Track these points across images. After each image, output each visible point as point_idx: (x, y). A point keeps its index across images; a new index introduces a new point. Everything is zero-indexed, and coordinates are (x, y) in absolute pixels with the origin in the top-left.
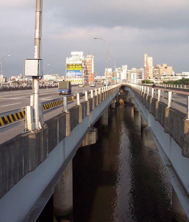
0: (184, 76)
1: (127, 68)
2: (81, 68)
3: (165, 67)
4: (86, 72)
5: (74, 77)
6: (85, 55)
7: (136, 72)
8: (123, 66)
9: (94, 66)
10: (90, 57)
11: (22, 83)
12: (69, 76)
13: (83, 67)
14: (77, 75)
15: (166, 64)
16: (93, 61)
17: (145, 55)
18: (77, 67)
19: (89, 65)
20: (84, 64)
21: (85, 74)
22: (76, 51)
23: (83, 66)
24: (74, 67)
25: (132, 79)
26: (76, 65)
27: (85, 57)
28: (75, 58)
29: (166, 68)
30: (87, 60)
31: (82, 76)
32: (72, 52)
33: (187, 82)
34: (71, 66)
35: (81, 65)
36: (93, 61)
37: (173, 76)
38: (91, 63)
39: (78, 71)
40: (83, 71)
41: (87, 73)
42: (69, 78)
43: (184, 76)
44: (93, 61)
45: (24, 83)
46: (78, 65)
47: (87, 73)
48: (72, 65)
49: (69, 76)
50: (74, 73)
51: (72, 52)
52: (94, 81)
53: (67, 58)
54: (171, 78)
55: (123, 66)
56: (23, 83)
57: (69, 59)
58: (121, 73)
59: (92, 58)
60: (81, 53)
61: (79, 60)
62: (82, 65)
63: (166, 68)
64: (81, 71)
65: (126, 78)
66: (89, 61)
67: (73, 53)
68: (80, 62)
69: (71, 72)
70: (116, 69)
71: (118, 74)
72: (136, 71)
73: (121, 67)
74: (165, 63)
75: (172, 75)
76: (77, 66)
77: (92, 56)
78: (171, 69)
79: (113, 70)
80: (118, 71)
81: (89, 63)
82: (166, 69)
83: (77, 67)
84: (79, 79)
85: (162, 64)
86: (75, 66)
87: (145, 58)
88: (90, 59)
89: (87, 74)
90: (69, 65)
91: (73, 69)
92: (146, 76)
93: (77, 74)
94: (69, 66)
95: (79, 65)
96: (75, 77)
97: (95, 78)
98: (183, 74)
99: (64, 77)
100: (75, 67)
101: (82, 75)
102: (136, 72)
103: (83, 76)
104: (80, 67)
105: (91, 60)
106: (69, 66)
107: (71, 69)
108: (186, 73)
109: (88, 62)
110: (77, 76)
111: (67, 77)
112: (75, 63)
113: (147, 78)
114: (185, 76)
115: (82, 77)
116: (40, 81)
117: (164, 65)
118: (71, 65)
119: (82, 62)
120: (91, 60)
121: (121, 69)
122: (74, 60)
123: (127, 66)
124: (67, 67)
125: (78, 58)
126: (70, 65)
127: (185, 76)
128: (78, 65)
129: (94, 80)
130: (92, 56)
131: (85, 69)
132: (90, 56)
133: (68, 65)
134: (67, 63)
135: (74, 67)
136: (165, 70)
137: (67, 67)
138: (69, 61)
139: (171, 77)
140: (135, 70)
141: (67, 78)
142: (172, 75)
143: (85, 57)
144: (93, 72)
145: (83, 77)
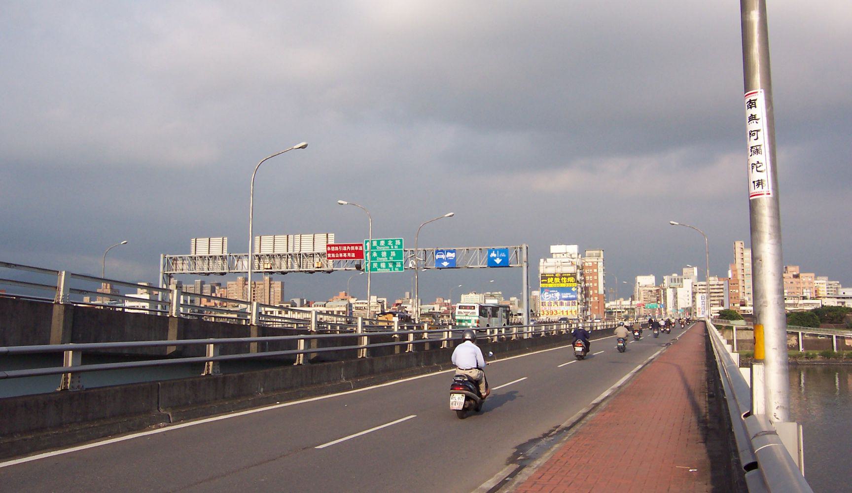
0: (844, 298)
1: (696, 274)
2: (575, 282)
3: (795, 273)
4: (584, 292)
5: (558, 304)
6: (582, 253)
7: (718, 287)
8: (685, 270)
9: (604, 277)
10: (594, 255)
11: (440, 317)
12: (547, 302)
13: (578, 281)
14: (565, 299)
15: (798, 267)
16: (602, 263)
17: (738, 245)
18: (565, 281)
19: (590, 274)
20: (582, 274)
21: (583, 297)
22: (561, 244)
23: (579, 277)
24: (557, 280)
25: (698, 306)
26: (561, 276)
27: (584, 256)
28: (560, 259)
29: (796, 276)
30: (589, 262)
31: (576, 301)
32: (551, 246)
33: (831, 314)
34: (552, 279)
35: (574, 275)
36: (600, 264)
37: (807, 299)
38: (595, 270)
39: (568, 290)
40: (579, 290)
41: (586, 291)
42: (547, 305)
43: (844, 298)
44: (602, 265)
45: (445, 317)
46: (567, 277)
47: (586, 291)
48: (553, 275)
49: (547, 302)
50: (558, 295)
51: (551, 246)
52: (605, 312)
53: (542, 260)
54: (801, 305)
55: (685, 270)
56: (443, 316)
57: (546, 264)
58: (679, 290)
59: (599, 256)
60: (573, 249)
61: (570, 264)
62: (575, 277)
63: (796, 276)
64: (574, 289)
65: (690, 305)
66: (591, 264)
67: (554, 249)
68: (572, 270)
69: (551, 293)
70: (666, 278)
71: (670, 293)
72: (717, 285)
73: (681, 273)
74: (794, 265)
75: (804, 298)
76: (565, 278)
77: (598, 252)
78: (810, 279)
79: (659, 281)
80: (673, 285)
81: (593, 271)
82: (797, 280)
83: (565, 281)
84: (569, 308)
85: (786, 268)
86: (560, 278)
87: (738, 250)
88: (596, 260)
89: (586, 295)
90: (547, 275)
91: (555, 285)
92: (732, 300)
93: (565, 296)
94: (546, 278)
95: (570, 277)
96: (562, 304)
97: (607, 305)
98: (841, 294)
99: (515, 298)
100: (561, 281)
101: (576, 299)
102: (718, 287)
103: (579, 302)
104: (571, 279)
105: (596, 263)
106: (546, 278)
107: (551, 286)
108: (850, 292)
109: (589, 267)
110: (565, 302)
111: (542, 303)
112: (559, 271)
113: (736, 305)
114: (848, 298)
115: (576, 304)
116: (394, 307)
117: (790, 269)
118: (550, 277)
119: (576, 269)
120: (596, 263)
121: (680, 277)
122: (557, 264)
123: (695, 269)
124: (542, 281)
125: (567, 260)
126: (549, 275)
127: (848, 298)
128: (567, 277)
129: (605, 310)
130: (600, 254)
131: (583, 285)
132: (594, 252)
133: (545, 277)
134: (542, 270)
135: (557, 280)
136: (794, 282)
137: (542, 281)
138: (546, 266)
139: (801, 302)
140: (716, 283)
141: (541, 306)
142: (804, 298)
143: (584, 256)
144: (601, 290)
145: (578, 304)
